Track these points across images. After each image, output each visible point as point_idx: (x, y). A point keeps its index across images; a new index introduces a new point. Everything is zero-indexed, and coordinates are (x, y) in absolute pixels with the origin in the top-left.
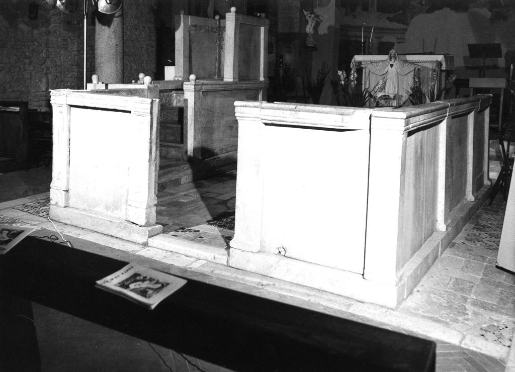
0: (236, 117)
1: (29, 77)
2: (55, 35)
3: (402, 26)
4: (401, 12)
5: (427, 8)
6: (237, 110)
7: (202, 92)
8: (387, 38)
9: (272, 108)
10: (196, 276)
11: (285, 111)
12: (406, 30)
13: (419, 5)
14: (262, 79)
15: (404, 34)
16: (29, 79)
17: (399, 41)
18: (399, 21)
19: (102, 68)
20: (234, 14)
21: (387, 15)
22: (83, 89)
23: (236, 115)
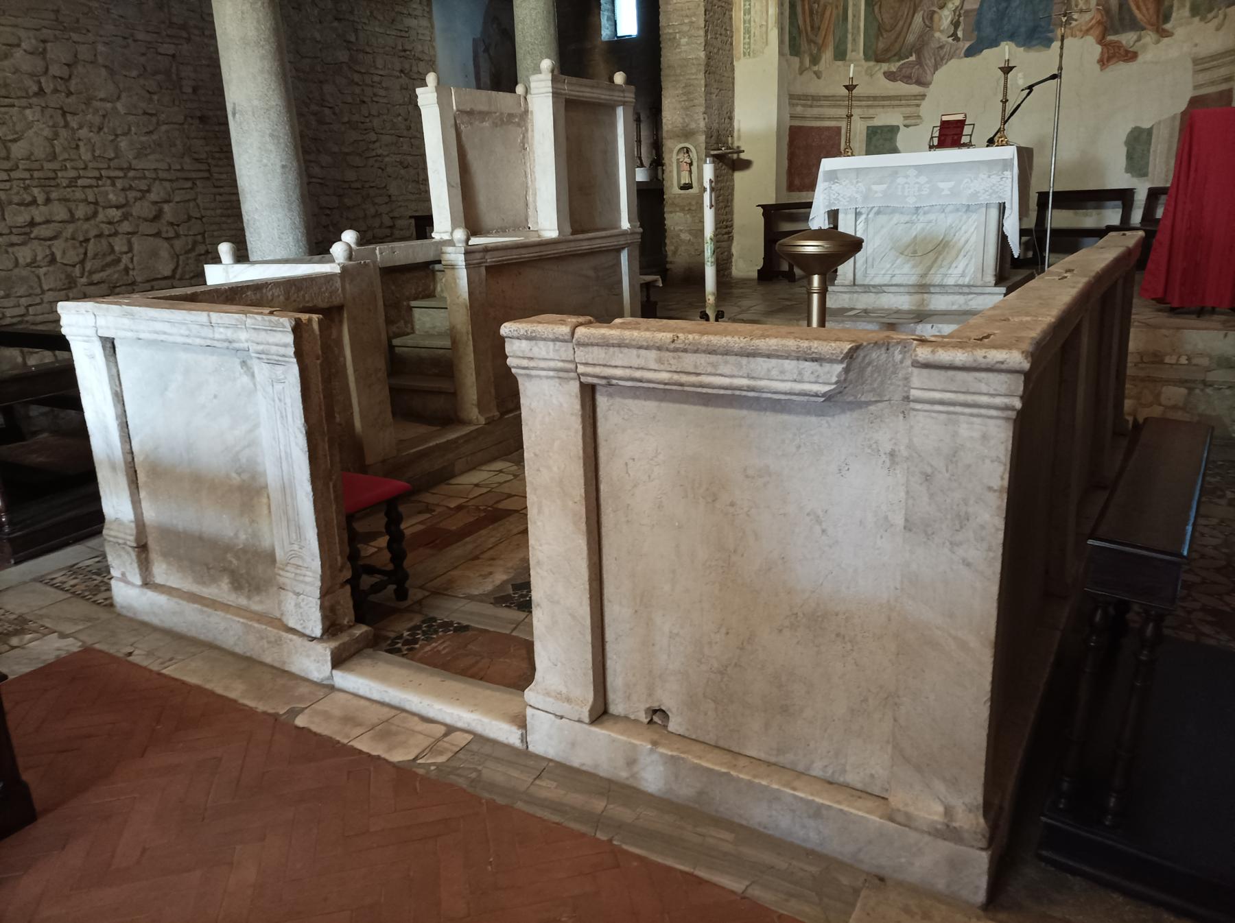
0: (509, 369)
1: (125, 249)
2: (173, 150)
3: (915, 89)
4: (913, 58)
5: (967, 44)
6: (510, 348)
7: (486, 267)
8: (885, 118)
9: (605, 344)
10: (629, 323)
11: (642, 352)
12: (923, 96)
13: (950, 39)
14: (625, 225)
15: (918, 106)
16: (126, 253)
17: (907, 122)
18: (907, 79)
19: (258, 224)
20: (549, 76)
21: (885, 67)
22: (839, 129)
23: (510, 361)
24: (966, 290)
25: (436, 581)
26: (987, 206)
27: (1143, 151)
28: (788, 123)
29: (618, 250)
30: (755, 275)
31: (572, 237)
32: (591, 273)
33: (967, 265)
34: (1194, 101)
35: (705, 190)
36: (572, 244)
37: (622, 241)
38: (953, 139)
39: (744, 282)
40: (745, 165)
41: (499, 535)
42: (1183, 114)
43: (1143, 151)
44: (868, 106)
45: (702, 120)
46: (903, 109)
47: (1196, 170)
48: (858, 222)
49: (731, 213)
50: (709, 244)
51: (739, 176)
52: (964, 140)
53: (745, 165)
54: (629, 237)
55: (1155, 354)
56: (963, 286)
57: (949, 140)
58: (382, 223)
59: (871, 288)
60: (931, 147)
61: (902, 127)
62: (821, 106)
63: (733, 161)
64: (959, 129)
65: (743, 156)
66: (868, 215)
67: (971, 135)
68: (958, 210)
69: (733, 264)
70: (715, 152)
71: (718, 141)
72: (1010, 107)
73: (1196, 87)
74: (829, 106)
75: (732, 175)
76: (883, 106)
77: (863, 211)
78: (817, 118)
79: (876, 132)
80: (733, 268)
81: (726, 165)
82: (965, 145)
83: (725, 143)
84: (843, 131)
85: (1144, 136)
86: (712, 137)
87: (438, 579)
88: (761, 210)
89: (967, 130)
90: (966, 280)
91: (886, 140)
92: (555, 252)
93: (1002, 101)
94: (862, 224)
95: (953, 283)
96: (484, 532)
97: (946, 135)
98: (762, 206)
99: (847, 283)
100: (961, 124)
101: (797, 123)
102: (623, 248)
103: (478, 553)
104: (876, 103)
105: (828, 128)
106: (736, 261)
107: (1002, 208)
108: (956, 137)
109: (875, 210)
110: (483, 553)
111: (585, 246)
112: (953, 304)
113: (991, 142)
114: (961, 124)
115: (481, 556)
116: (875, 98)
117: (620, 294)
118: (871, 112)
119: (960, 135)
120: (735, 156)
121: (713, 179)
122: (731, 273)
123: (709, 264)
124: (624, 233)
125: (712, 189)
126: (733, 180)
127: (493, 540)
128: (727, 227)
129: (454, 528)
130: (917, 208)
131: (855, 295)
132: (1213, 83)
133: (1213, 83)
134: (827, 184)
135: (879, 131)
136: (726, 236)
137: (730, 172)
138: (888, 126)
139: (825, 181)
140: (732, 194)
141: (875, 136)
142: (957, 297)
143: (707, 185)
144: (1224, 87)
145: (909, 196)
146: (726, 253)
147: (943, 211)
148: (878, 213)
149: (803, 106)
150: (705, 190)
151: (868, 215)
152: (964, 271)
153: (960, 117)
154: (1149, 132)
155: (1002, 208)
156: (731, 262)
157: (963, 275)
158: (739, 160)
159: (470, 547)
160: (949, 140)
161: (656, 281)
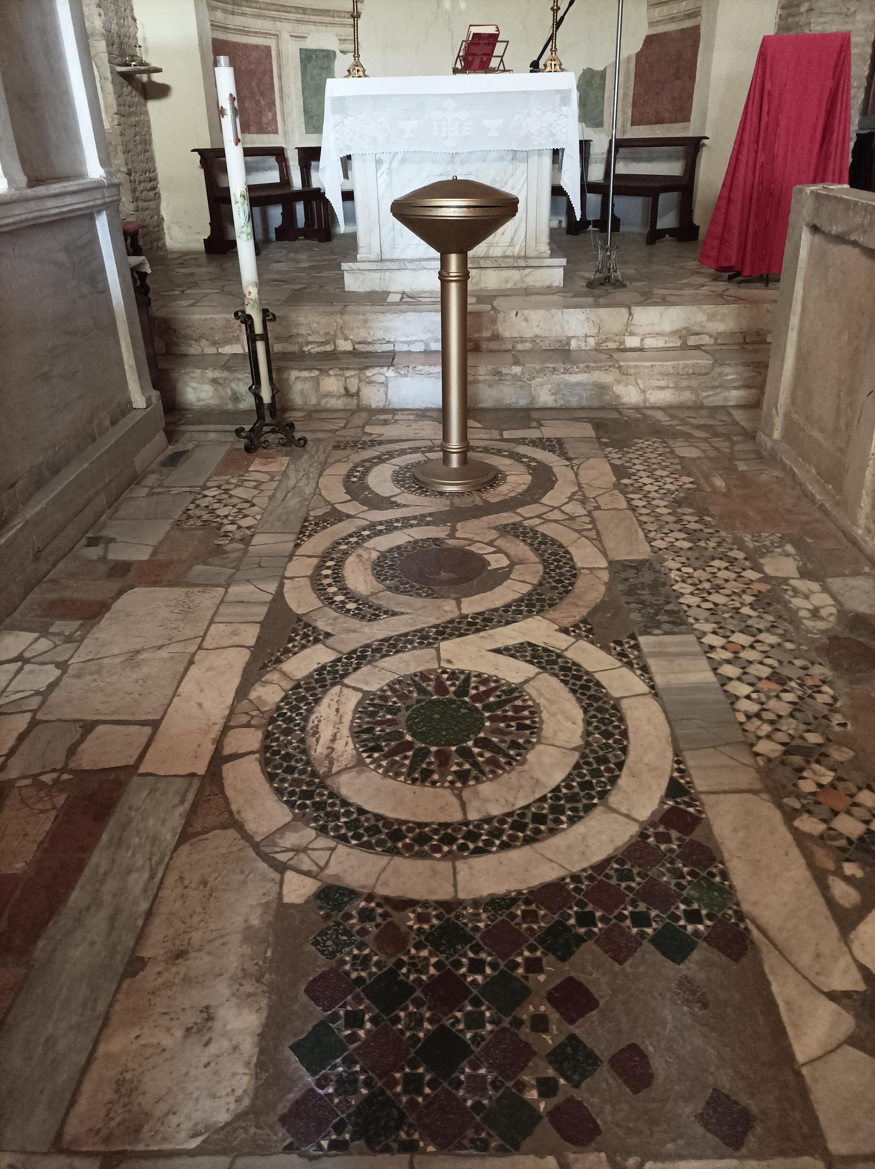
22: (268, 49)
24: (522, 263)
25: (83, 1101)
26: (540, 152)
27: (597, 97)
28: (209, 34)
29: (89, 216)
30: (201, 247)
31: (30, 192)
32: (62, 257)
33: (516, 231)
34: (650, 41)
35: (221, 112)
36: (33, 205)
37: (97, 199)
38: (481, 61)
39: (185, 257)
40: (162, 91)
41: (139, 861)
42: (638, 55)
43: (597, 97)
44: (299, 21)
45: (97, 16)
46: (337, 29)
47: (768, 113)
48: (379, 175)
49: (151, 160)
50: (239, 204)
51: (154, 107)
52: (494, 63)
53: (162, 91)
54: (107, 193)
55: (758, 334)
56: (513, 257)
57: (477, 63)
58: (814, 593)
59: (407, 263)
60: (455, 71)
61: (338, 53)
62: (243, 14)
63: (144, 85)
64: (491, 47)
65: (156, 78)
66: (390, 164)
67: (502, 57)
68: (502, 159)
69: (166, 231)
70: (124, 69)
71: (122, 54)
72: (560, 14)
73: (651, 24)
74: (254, 16)
75: (146, 106)
76: (315, 23)
77: (384, 157)
78: (240, 30)
79: (311, 57)
80: (167, 237)
81: (136, 90)
82: (493, 71)
83: (133, 57)
84: (274, 53)
85: (597, 78)
86: (113, 45)
87: (87, 1087)
88: (197, 157)
89: (499, 49)
90: (516, 250)
91: (322, 69)
92: (11, 220)
93: (552, 9)
94: (384, 176)
95: (500, 254)
96: (98, 859)
97: (475, 54)
98: (201, 152)
99: (373, 257)
100: (492, 39)
101: (221, 36)
102: (99, 212)
103: (129, 940)
104: (306, 18)
105: (257, 47)
106: (169, 227)
107: (557, 154)
108: (485, 59)
109: (399, 157)
110: (141, 936)
111: (53, 207)
112: (507, 281)
113: (535, 67)
114: (492, 39)
115: (146, 954)
116: (304, 10)
117: (105, 291)
118: (302, 29)
119: (490, 55)
120: (145, 78)
121: (235, 95)
122: (164, 245)
123: (244, 236)
124: (97, 187)
125: (235, 112)
126: (146, 113)
127: (137, 881)
128: (151, 180)
129: (20, 865)
130: (454, 155)
131: (388, 274)
132: (672, 19)
133: (672, 19)
134: (337, 117)
135: (314, 56)
136: (152, 193)
137: (142, 100)
138: (323, 51)
139: (334, 112)
140: (149, 133)
141: (310, 62)
142: (512, 272)
143: (225, 103)
144: (687, 24)
145: (447, 138)
146: (156, 217)
147: (484, 161)
148: (404, 161)
149: (225, 11)
150: (221, 112)
151: (390, 164)
152: (512, 239)
153: (492, 30)
154: (603, 74)
155: (557, 154)
156: (163, 229)
157: (512, 244)
158: (151, 83)
159: (97, 923)
160: (477, 63)
161: (141, 264)
